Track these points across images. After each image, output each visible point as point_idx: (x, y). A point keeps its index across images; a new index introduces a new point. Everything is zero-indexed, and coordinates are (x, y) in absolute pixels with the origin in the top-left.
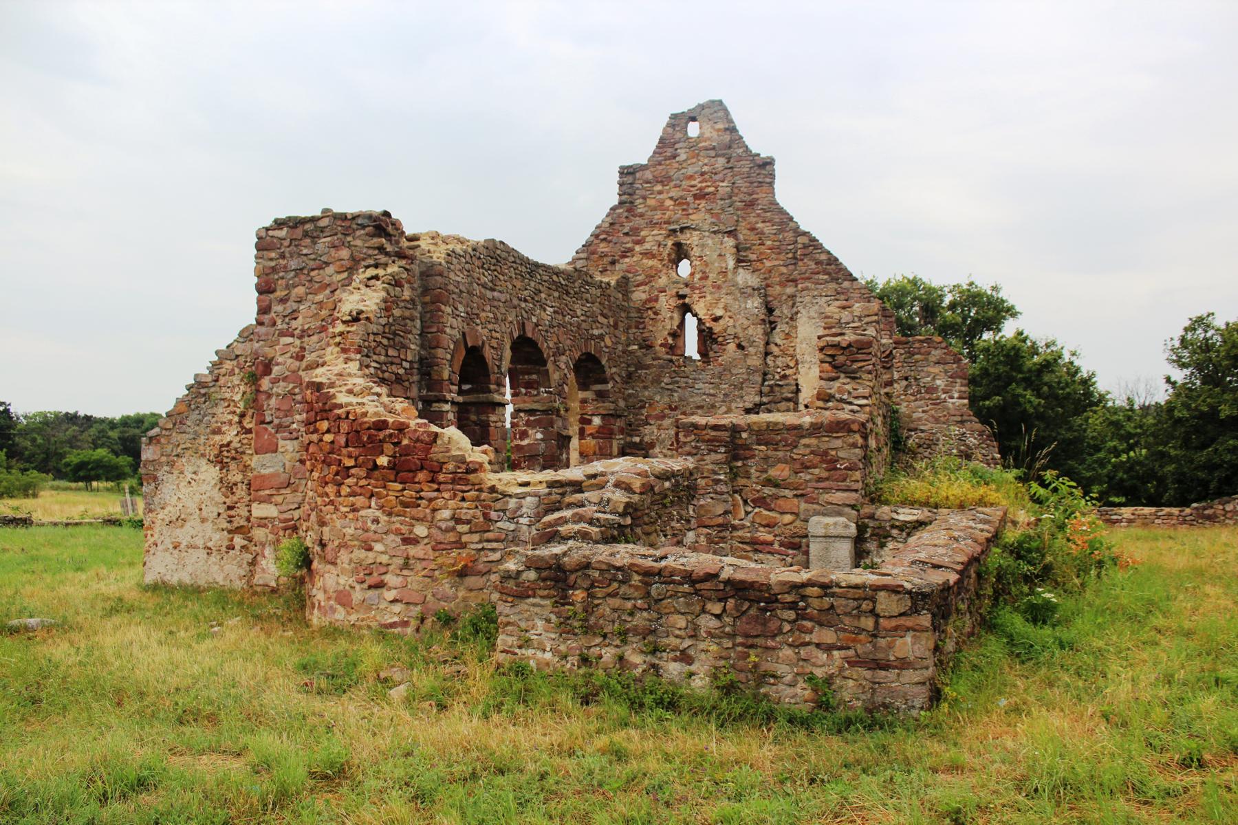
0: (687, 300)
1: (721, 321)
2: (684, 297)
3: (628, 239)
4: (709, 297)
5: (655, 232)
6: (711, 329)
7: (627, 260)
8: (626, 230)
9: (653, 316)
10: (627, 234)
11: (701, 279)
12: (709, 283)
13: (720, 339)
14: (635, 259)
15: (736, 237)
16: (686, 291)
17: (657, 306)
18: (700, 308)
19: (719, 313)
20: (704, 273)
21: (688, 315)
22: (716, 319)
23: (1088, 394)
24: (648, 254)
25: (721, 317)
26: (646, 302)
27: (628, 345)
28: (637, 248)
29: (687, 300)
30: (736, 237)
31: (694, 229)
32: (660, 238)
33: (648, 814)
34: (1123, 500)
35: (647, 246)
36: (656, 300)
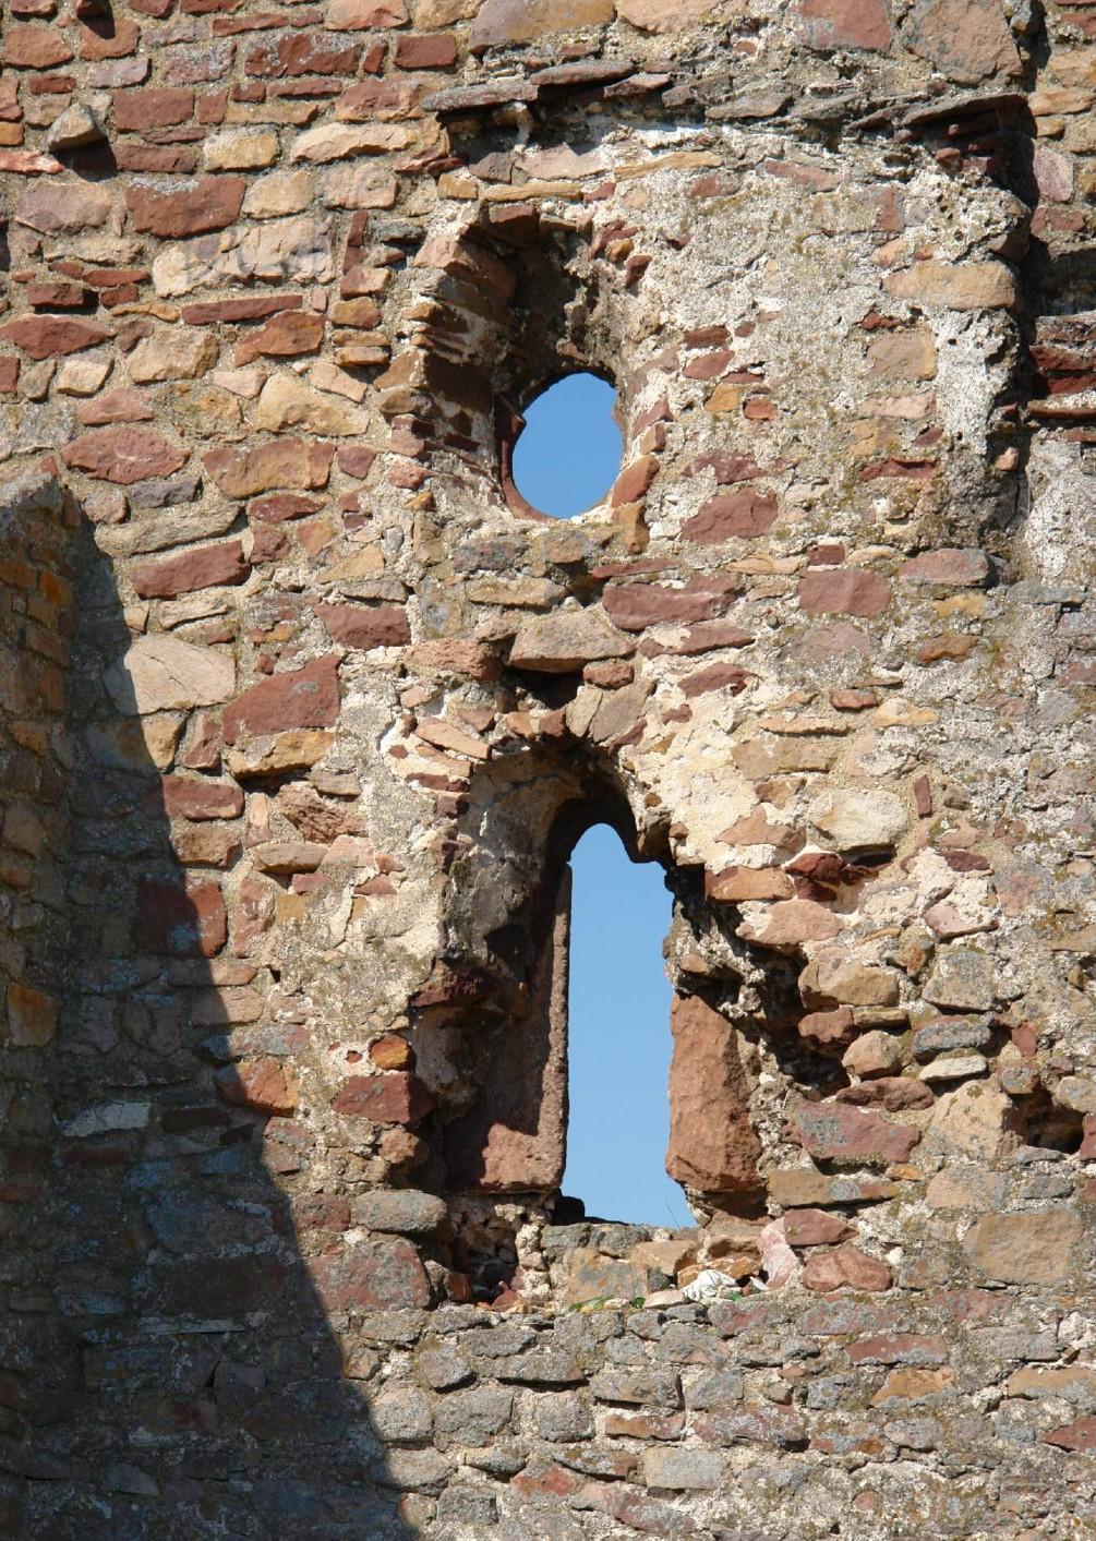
0: (584, 710)
1: (881, 901)
2: (556, 682)
3: (88, 195)
4: (768, 692)
5: (327, 136)
6: (783, 961)
7: (83, 370)
8: (71, 123)
9: (291, 847)
10: (88, 155)
11: (699, 529)
12: (776, 556)
13: (865, 1052)
14: (148, 360)
15: (1014, 174)
16: (581, 629)
17: (327, 754)
18: (696, 776)
19: (863, 818)
20: (735, 470)
21: (597, 849)
22: (839, 876)
23: (455, 997)
24: (257, 318)
25: (873, 858)
26: (234, 717)
27: (73, 1092)
28: (171, 269)
29: (584, 710)
30: (1014, 174)
31: (652, 106)
32: (361, 185)
33: (957, 827)
34: (560, 920)
35: (260, 249)
36: (320, 703)
